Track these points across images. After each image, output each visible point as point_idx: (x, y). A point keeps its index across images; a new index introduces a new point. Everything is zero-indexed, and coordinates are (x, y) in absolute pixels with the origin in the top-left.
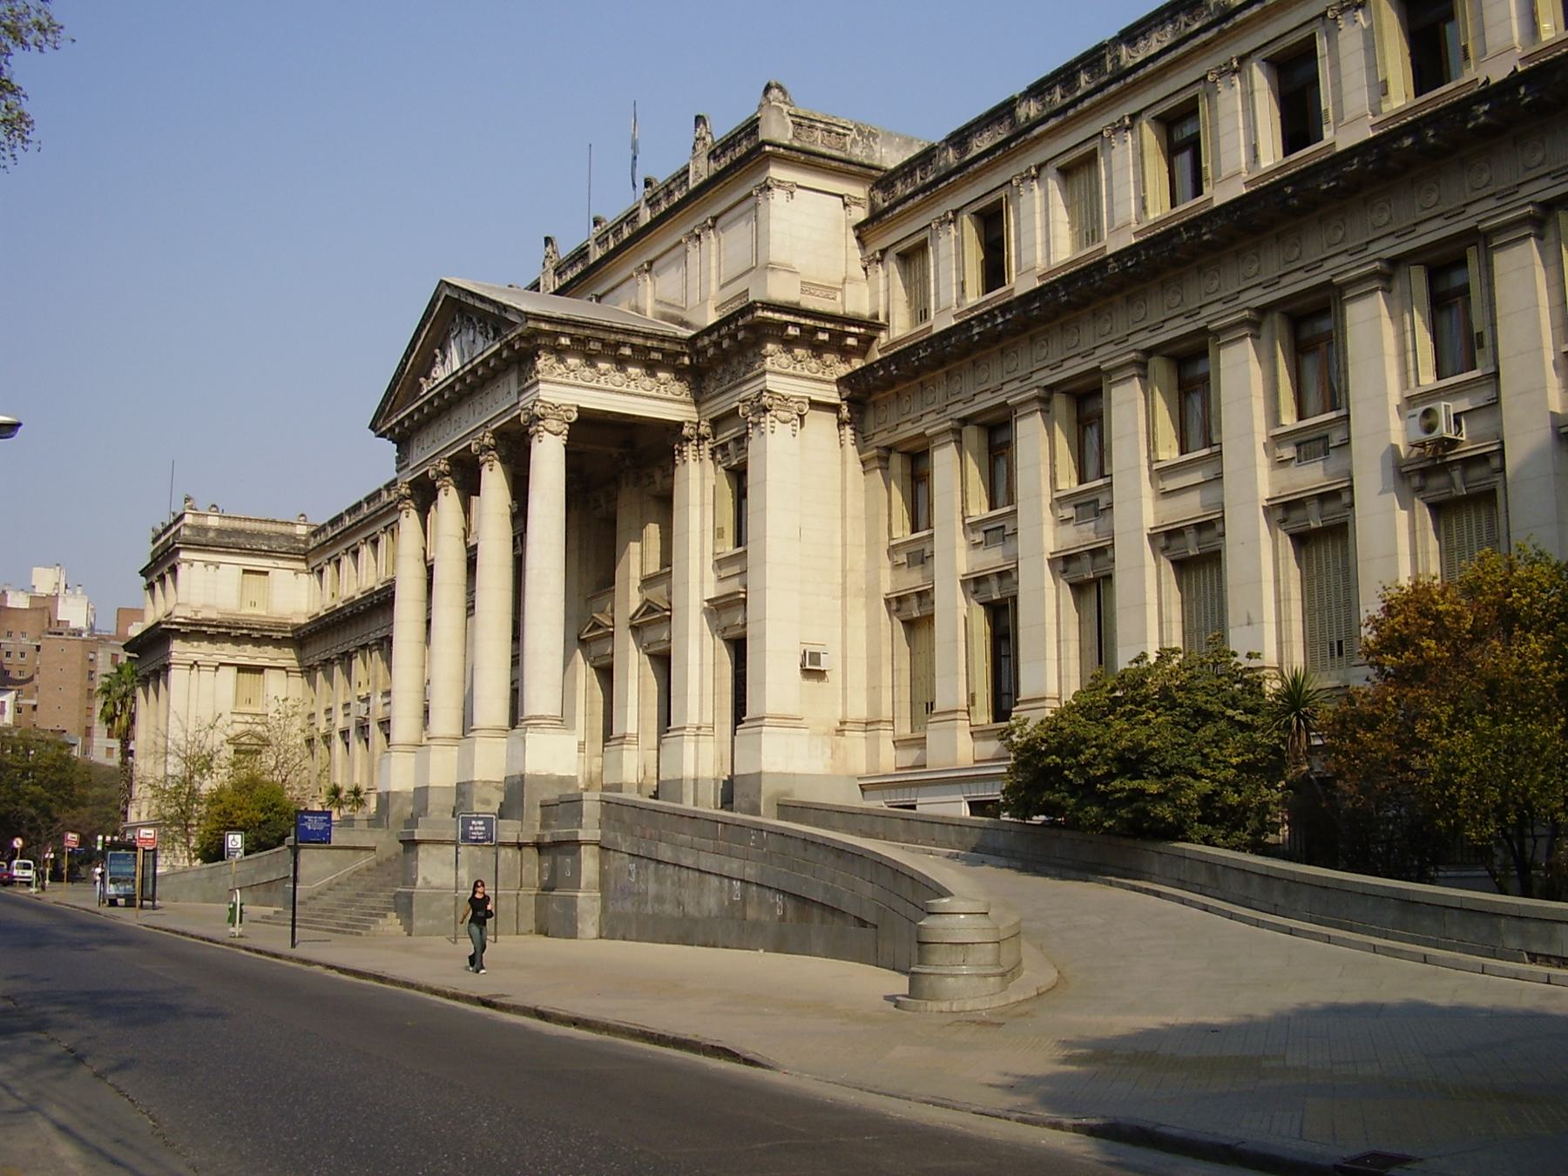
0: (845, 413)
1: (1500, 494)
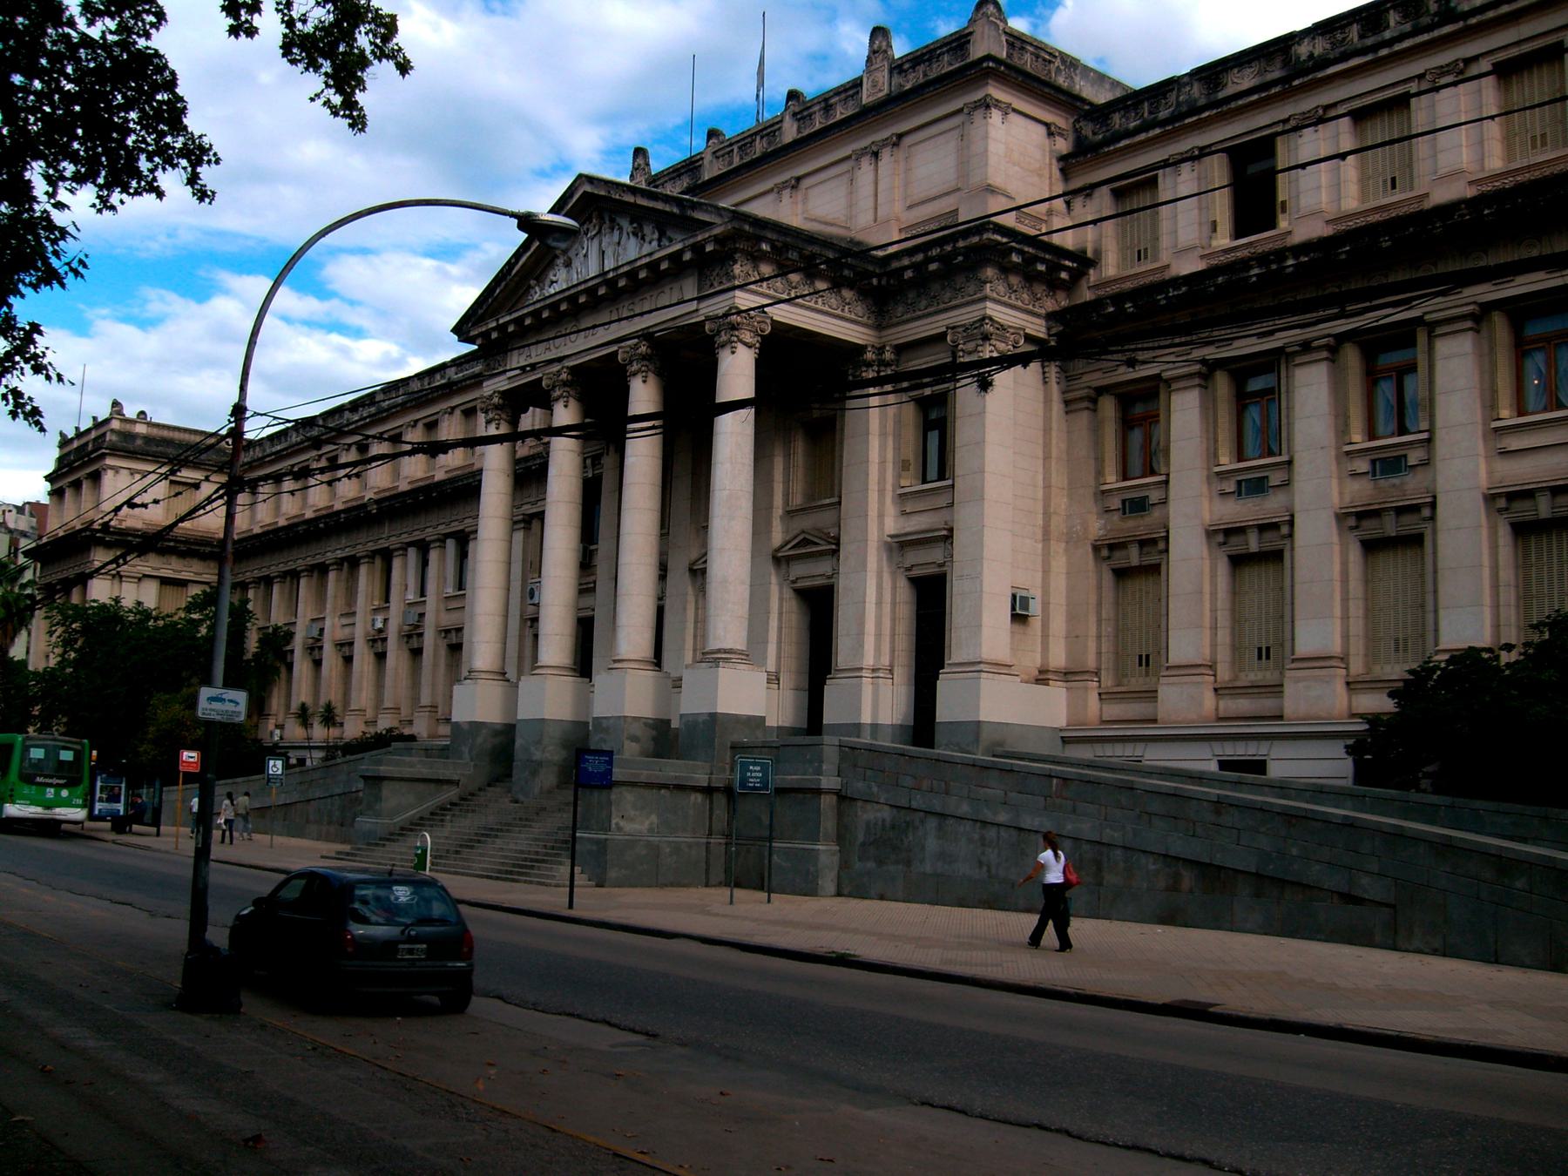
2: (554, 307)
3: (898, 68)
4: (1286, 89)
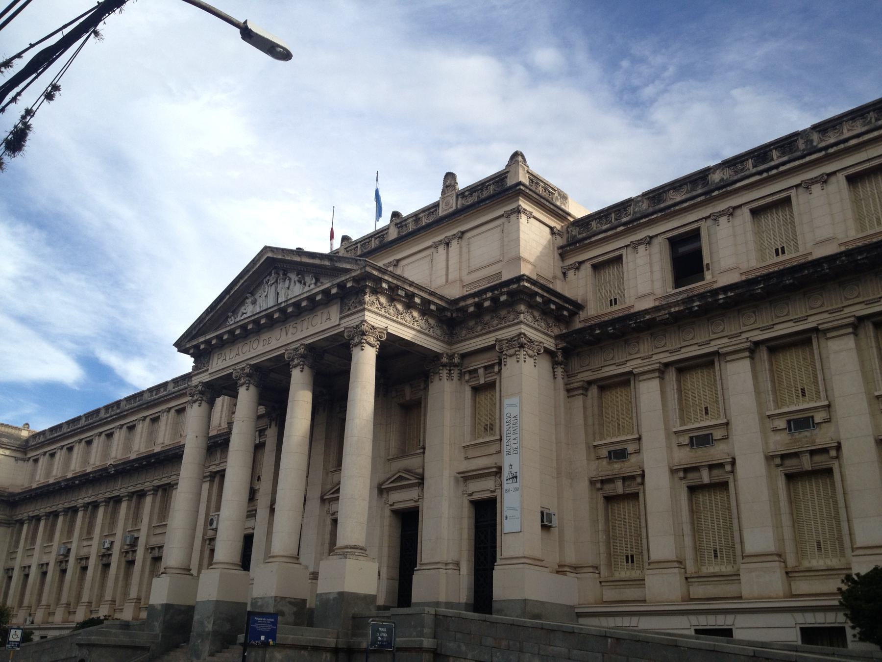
0: (560, 357)
1: (641, 495)
2: (244, 327)
3: (462, 194)
4: (709, 198)
